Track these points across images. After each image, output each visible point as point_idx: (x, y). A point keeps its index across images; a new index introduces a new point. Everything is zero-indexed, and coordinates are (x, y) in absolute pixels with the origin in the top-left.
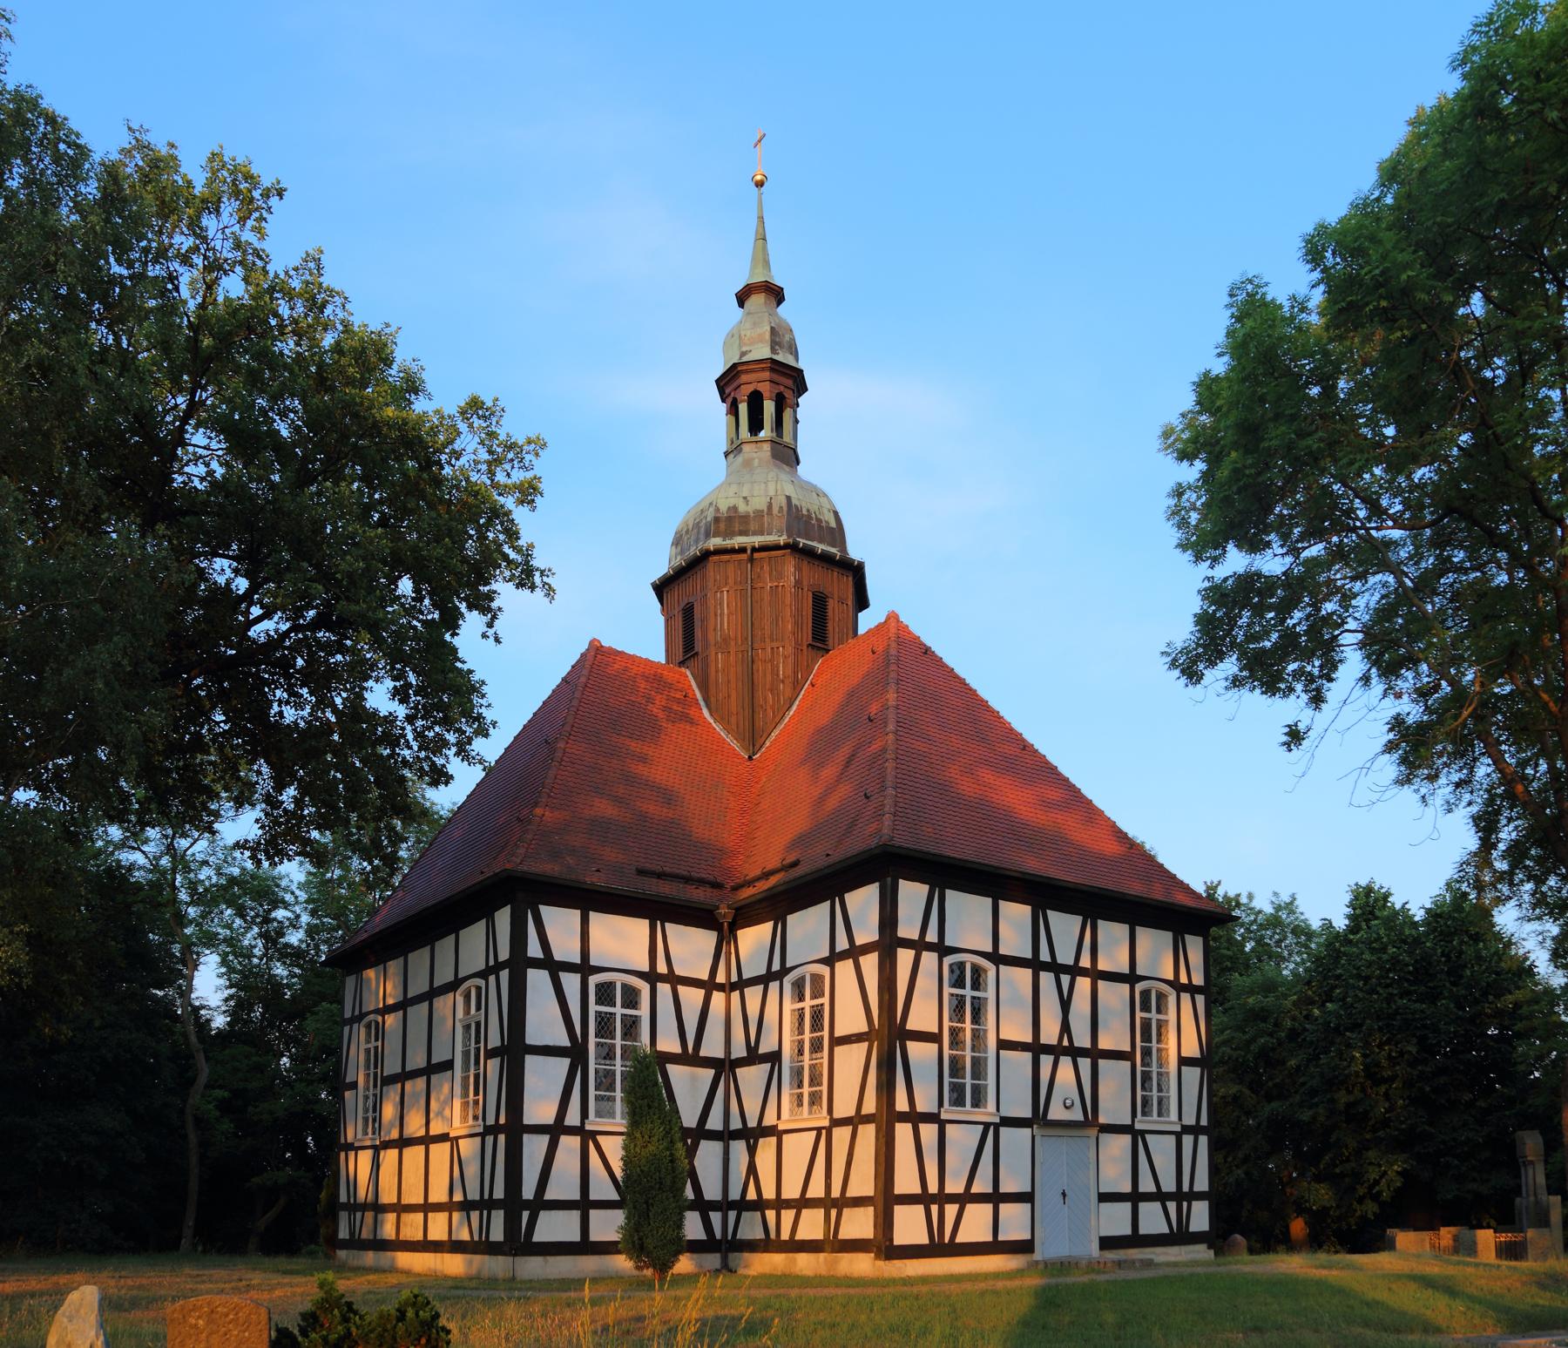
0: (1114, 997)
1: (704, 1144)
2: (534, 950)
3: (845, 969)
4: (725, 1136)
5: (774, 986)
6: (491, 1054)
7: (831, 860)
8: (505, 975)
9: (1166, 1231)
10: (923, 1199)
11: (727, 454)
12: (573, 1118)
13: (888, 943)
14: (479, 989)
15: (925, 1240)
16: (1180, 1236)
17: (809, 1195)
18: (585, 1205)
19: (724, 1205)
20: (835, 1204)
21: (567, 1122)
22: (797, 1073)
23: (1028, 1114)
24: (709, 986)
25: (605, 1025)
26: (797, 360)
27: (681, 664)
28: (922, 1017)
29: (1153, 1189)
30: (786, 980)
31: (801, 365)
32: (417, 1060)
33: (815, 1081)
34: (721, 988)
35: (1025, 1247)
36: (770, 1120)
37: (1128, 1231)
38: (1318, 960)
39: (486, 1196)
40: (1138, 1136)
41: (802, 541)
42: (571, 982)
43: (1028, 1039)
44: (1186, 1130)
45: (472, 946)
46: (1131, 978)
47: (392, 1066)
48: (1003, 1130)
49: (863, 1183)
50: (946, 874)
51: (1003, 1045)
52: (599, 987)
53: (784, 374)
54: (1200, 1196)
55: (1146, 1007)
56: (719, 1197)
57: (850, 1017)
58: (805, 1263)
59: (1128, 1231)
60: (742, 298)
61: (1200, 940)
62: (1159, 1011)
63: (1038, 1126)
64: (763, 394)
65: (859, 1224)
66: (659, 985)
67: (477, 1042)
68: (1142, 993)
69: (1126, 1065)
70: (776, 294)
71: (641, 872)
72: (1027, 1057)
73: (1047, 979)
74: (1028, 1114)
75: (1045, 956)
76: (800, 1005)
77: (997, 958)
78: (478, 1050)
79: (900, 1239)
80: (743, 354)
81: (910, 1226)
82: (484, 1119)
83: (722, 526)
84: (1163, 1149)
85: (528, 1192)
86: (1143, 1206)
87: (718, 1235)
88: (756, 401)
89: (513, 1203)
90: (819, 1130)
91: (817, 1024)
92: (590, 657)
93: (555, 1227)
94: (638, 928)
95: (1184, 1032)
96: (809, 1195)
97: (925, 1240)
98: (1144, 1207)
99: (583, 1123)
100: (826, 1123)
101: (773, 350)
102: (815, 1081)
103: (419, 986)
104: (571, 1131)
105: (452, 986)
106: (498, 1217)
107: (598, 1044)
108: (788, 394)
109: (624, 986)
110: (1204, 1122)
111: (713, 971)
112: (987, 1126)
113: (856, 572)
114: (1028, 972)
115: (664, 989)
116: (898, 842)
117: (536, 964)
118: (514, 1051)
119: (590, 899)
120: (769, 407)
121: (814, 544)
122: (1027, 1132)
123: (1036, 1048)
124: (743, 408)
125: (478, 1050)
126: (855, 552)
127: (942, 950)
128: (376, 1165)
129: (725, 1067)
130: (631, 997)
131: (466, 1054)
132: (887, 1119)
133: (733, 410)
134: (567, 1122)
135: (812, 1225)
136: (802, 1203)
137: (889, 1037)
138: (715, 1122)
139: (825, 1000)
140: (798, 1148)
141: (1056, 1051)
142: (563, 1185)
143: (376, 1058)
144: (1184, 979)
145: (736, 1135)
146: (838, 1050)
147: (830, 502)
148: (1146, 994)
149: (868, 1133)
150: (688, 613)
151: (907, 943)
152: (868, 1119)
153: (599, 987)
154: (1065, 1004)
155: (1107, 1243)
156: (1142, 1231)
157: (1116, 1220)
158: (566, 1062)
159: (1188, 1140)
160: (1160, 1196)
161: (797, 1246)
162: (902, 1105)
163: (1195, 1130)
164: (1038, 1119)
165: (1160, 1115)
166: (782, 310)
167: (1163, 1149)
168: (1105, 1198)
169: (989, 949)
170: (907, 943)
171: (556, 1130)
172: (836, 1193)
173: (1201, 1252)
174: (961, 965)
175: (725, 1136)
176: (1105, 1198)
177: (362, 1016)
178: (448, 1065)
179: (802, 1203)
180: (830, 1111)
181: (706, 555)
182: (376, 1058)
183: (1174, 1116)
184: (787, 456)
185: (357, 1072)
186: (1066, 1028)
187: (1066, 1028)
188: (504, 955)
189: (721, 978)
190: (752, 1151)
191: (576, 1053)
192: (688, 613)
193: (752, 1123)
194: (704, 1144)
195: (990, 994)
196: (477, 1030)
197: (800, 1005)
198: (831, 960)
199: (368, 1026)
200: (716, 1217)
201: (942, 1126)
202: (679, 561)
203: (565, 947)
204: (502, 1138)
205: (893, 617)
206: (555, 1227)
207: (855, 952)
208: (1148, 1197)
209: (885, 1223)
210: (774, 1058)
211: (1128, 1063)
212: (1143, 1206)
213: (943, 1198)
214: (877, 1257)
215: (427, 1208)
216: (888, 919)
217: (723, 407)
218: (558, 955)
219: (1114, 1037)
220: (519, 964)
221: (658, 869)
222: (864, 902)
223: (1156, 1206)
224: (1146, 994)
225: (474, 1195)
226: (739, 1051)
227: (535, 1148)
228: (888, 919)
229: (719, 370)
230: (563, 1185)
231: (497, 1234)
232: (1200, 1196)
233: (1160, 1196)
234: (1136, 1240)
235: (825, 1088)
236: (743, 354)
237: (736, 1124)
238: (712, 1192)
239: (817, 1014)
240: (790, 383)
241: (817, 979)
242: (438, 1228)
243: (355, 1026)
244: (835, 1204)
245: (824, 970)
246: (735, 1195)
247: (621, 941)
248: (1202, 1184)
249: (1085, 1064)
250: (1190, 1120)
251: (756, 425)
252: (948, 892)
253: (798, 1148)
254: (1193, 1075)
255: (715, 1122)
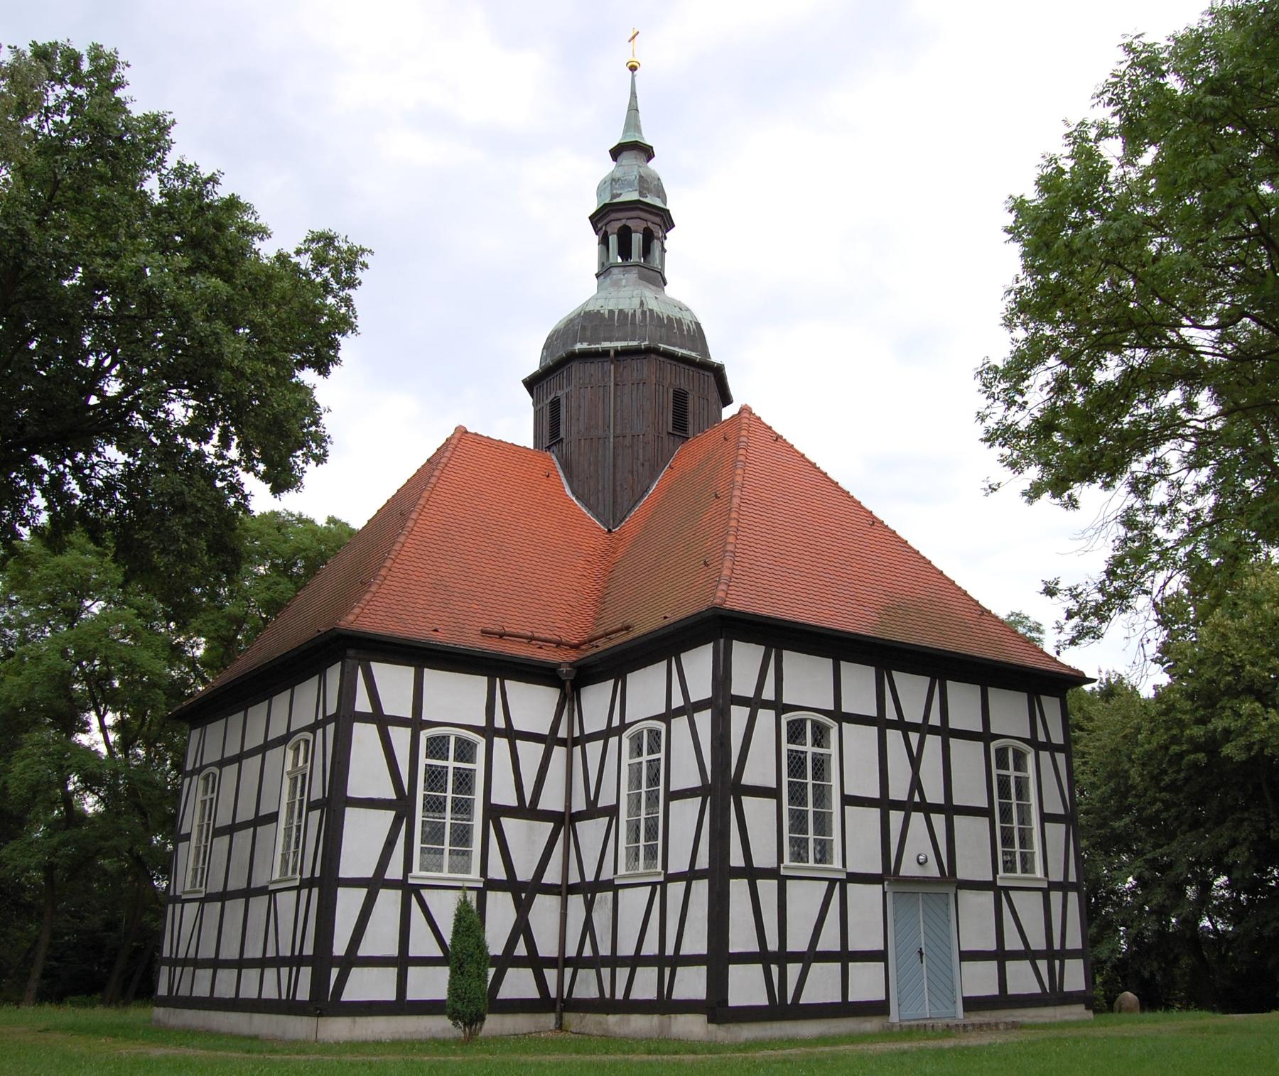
0: (968, 757)
1: (539, 899)
2: (362, 704)
3: (680, 725)
4: (563, 890)
5: (613, 741)
6: (312, 806)
7: (666, 622)
8: (331, 728)
9: (1039, 991)
10: (762, 957)
11: (598, 276)
12: (395, 871)
13: (721, 702)
14: (307, 742)
15: (763, 1000)
16: (1054, 996)
17: (644, 952)
18: (403, 961)
19: (560, 962)
20: (669, 962)
21: (388, 876)
22: (634, 829)
23: (878, 869)
24: (549, 740)
25: (435, 778)
26: (665, 202)
27: (549, 448)
28: (759, 770)
29: (1019, 946)
30: (625, 736)
31: (668, 207)
32: (246, 814)
33: (651, 833)
34: (562, 743)
35: (878, 1008)
36: (606, 875)
37: (995, 991)
38: (89, 748)
39: (297, 953)
40: (1000, 893)
41: (662, 346)
42: (400, 737)
43: (876, 794)
44: (1053, 886)
45: (305, 703)
46: (985, 736)
47: (224, 819)
48: (850, 886)
49: (696, 942)
50: (780, 636)
51: (847, 800)
52: (431, 741)
53: (651, 213)
54: (1073, 954)
55: (1002, 764)
56: (555, 954)
57: (685, 774)
58: (640, 1024)
59: (995, 991)
60: (616, 153)
61: (1057, 701)
62: (1017, 768)
63: (906, 886)
64: (632, 227)
65: (692, 984)
66: (496, 739)
67: (302, 794)
68: (997, 751)
69: (985, 821)
70: (648, 152)
71: (485, 633)
72: (875, 813)
73: (894, 737)
74: (878, 869)
75: (891, 714)
76: (638, 760)
77: (839, 716)
78: (301, 802)
79: (735, 1000)
80: (614, 196)
81: (746, 986)
82: (301, 873)
83: (588, 333)
84: (1029, 906)
85: (340, 948)
86: (1010, 965)
87: (553, 993)
88: (625, 237)
89: (322, 959)
90: (654, 885)
91: (653, 780)
92: (454, 441)
93: (368, 985)
94: (476, 686)
95: (1045, 785)
96: (644, 952)
97: (763, 1000)
98: (390, 975)
99: (995, 877)
100: (661, 879)
101: (641, 194)
102: (651, 833)
103: (255, 740)
104: (392, 884)
105: (283, 740)
106: (306, 973)
107: (790, 783)
108: (655, 228)
109: (458, 740)
110: (1073, 878)
111: (555, 727)
112: (832, 882)
113: (718, 373)
114: (953, 724)
115: (501, 744)
116: (728, 605)
117: (364, 718)
118: (335, 803)
119: (422, 656)
120: (637, 239)
121: (676, 349)
122: (878, 889)
123: (884, 804)
124: (613, 240)
125: (301, 802)
126: (715, 358)
127: (779, 707)
128: (201, 914)
129: (564, 821)
130: (465, 751)
131: (291, 806)
132: (719, 874)
133: (604, 241)
134: (388, 876)
135: (646, 984)
136: (637, 961)
137: (723, 790)
138: (552, 876)
139: (661, 755)
140: (634, 902)
141: (907, 807)
142: (381, 938)
143: (210, 808)
144: (1042, 738)
145: (573, 889)
146: (672, 804)
147: (692, 314)
148: (1002, 753)
149: (701, 889)
150: (555, 405)
151: (742, 701)
152: (700, 875)
153: (431, 741)
154: (915, 761)
155: (972, 1004)
156: (1011, 990)
157: (980, 980)
158: (391, 815)
159: (1056, 897)
160: (1028, 954)
161: (630, 1006)
162: (736, 859)
163: (1064, 887)
164: (888, 875)
165: (1024, 870)
166: (651, 164)
167: (1029, 906)
168: (967, 956)
169: (830, 706)
170: (742, 701)
171: (375, 884)
172: (670, 951)
173: (1077, 1012)
174: (802, 722)
175: (563, 890)
176: (967, 956)
177: (202, 768)
178: (273, 817)
179: (637, 961)
180: (665, 866)
181: (573, 357)
182: (210, 808)
183: (1039, 873)
184: (657, 278)
185: (191, 821)
186: (916, 784)
187: (916, 784)
188: (332, 709)
189: (563, 733)
190: (589, 906)
191: (402, 806)
192: (555, 405)
193: (590, 877)
194: (539, 899)
195: (833, 750)
196: (300, 780)
197: (638, 760)
198: (668, 716)
199: (206, 778)
200: (551, 975)
201: (782, 881)
202: (550, 362)
203: (397, 701)
204: (315, 891)
205: (745, 410)
206: (368, 985)
207: (690, 709)
208: (1016, 956)
209: (718, 983)
210: (612, 812)
211: (986, 820)
212: (1010, 965)
213: (783, 957)
214: (710, 1021)
215: (845, 957)
216: (722, 676)
217: (596, 239)
218: (388, 710)
219: (971, 791)
220: (345, 718)
221: (498, 629)
222: (698, 666)
223: (1026, 965)
224: (1002, 753)
225: (286, 952)
226: (579, 804)
227: (348, 903)
228: (722, 676)
229: (593, 209)
230: (380, 939)
231: (303, 994)
232: (1073, 954)
233: (1028, 954)
234: (1003, 1000)
235: (660, 842)
236: (614, 196)
237: (574, 878)
238: (547, 948)
239: (653, 765)
240: (658, 220)
241: (654, 735)
242: (271, 985)
243: (195, 778)
244: (669, 962)
245: (661, 726)
246: (571, 951)
247: (456, 699)
248: (1075, 940)
249: (939, 820)
250: (1057, 876)
251: (625, 251)
252: (786, 654)
253: (634, 902)
254: (1057, 832)
255: (552, 876)
